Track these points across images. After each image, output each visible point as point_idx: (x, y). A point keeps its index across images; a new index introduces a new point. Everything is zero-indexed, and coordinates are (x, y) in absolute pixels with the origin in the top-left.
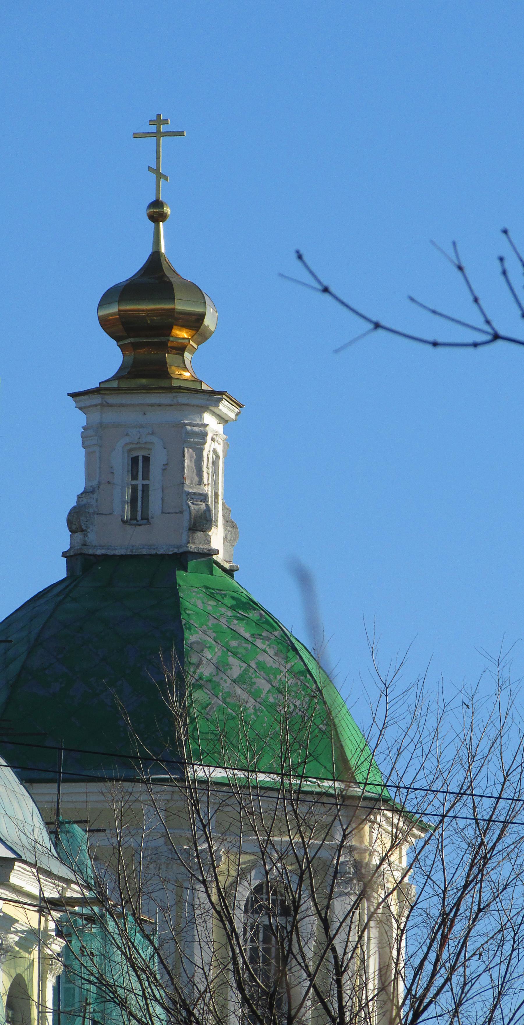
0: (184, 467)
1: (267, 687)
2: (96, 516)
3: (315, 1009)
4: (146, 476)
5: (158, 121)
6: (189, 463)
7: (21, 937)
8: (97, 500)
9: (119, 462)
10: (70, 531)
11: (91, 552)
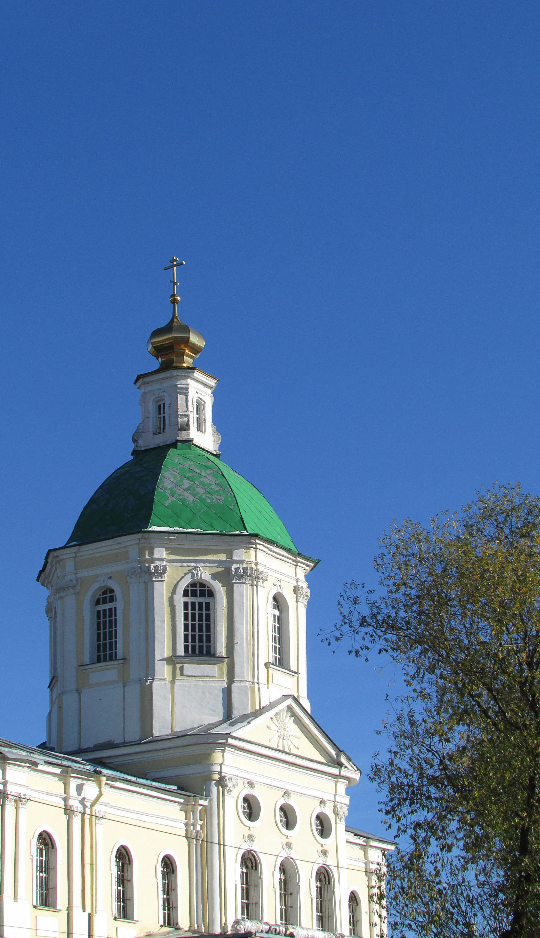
1: (203, 491)
7: (491, 700)
9: (152, 407)
11: (139, 449)
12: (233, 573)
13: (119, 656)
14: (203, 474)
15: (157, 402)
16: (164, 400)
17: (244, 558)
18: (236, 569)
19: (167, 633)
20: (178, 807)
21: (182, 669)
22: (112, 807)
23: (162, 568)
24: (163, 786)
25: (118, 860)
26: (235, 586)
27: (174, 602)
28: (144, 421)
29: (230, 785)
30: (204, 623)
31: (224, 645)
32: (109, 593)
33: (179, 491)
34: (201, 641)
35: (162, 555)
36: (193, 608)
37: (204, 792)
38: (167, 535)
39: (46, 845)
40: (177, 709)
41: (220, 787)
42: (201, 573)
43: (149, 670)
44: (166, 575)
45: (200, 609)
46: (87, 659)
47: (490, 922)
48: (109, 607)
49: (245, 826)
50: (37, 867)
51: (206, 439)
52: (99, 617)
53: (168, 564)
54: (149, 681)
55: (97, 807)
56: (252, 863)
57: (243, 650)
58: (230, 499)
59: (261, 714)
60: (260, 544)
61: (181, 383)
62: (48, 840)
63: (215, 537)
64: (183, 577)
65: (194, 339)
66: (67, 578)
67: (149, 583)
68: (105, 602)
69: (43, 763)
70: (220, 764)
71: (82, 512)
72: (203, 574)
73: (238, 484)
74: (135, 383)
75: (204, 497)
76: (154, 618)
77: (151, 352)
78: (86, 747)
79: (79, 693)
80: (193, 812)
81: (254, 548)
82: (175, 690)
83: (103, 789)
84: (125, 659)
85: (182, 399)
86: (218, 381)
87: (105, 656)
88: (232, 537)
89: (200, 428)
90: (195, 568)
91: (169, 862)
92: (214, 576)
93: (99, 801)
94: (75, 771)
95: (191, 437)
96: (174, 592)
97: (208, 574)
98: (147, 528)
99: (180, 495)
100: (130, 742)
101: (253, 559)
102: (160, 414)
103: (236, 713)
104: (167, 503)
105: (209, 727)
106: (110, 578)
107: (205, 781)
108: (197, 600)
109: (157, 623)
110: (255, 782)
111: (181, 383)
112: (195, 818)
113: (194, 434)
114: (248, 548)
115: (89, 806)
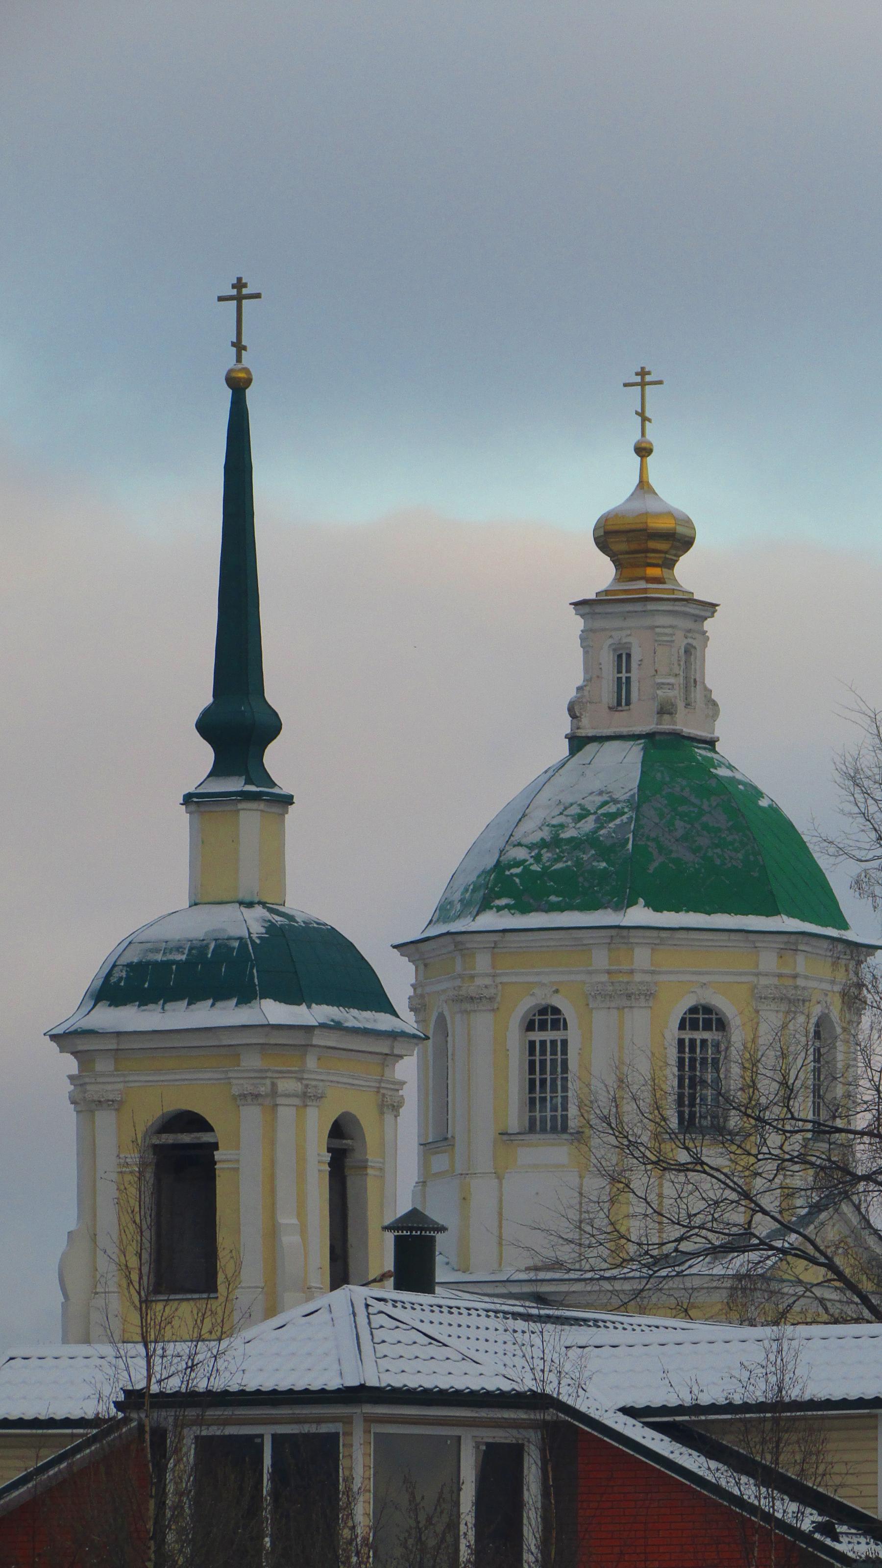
3: (849, 1109)
4: (628, 670)
5: (643, 373)
10: (714, 701)
15: (615, 650)
47: (788, 1128)
68: (543, 1027)
91: (550, 1415)
106: (557, 991)
108: (699, 1035)
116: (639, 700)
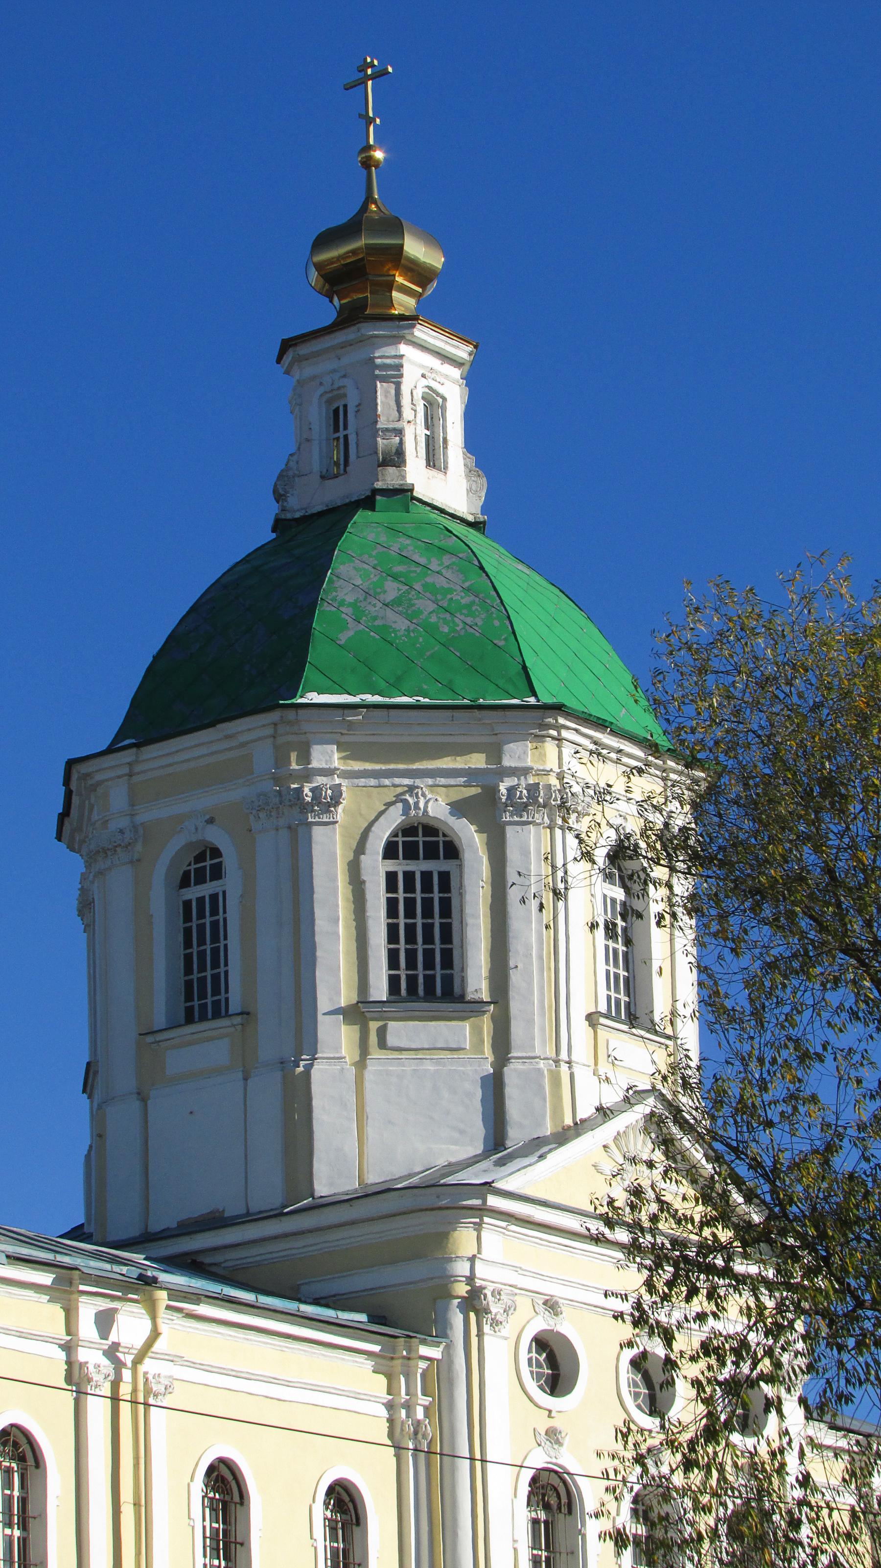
0: (377, 404)
1: (432, 607)
2: (296, 479)
6: (384, 399)
8: (297, 462)
9: (317, 416)
12: (504, 799)
13: (235, 1002)
14: (434, 566)
16: (345, 395)
17: (529, 762)
18: (511, 790)
19: (346, 946)
20: (368, 1364)
21: (382, 1033)
22: (193, 1365)
23: (329, 792)
24: (329, 1313)
25: (211, 1495)
26: (510, 831)
27: (363, 872)
28: (299, 448)
29: (495, 1308)
30: (437, 921)
31: (484, 972)
32: (211, 859)
33: (375, 608)
34: (429, 964)
35: (330, 760)
36: (409, 886)
37: (432, 1327)
38: (340, 711)
39: (22, 1459)
40: (371, 1131)
41: (472, 1315)
42: (427, 803)
43: (304, 1041)
44: (340, 809)
45: (427, 887)
46: (160, 1019)
48: (211, 892)
49: (540, 1407)
50: (326, 1559)
51: (449, 486)
52: (187, 917)
53: (345, 783)
54: (302, 1063)
55: (149, 1366)
56: (559, 1496)
57: (530, 983)
58: (497, 623)
59: (578, 1135)
60: (568, 728)
61: (383, 354)
62: (25, 1447)
63: (457, 714)
64: (381, 813)
65: (415, 248)
66: (113, 826)
67: (301, 830)
68: (201, 879)
69: (4, 1259)
70: (469, 1259)
71: (148, 670)
72: (430, 804)
73: (520, 586)
74: (279, 360)
75: (433, 619)
76: (313, 914)
77: (318, 288)
78: (159, 1228)
79: (143, 1098)
80: (407, 1376)
81: (553, 738)
82: (368, 1085)
83: (159, 1321)
84: (248, 1014)
85: (386, 393)
86: (476, 347)
87: (203, 1007)
88: (500, 713)
89: (434, 458)
90: (411, 789)
92: (459, 808)
93: (154, 1349)
94: (87, 1278)
95: (409, 480)
96: (360, 848)
97: (442, 802)
98: (294, 696)
99: (375, 618)
100: (261, 1212)
101: (552, 763)
102: (336, 429)
103: (515, 1136)
104: (343, 638)
105: (447, 1170)
106: (211, 821)
107: (435, 1300)
108: (418, 867)
109: (321, 923)
110: (561, 1301)
111: (383, 354)
112: (412, 1391)
113: (416, 474)
114: (540, 738)
115: (129, 1364)
116: (358, 457)
